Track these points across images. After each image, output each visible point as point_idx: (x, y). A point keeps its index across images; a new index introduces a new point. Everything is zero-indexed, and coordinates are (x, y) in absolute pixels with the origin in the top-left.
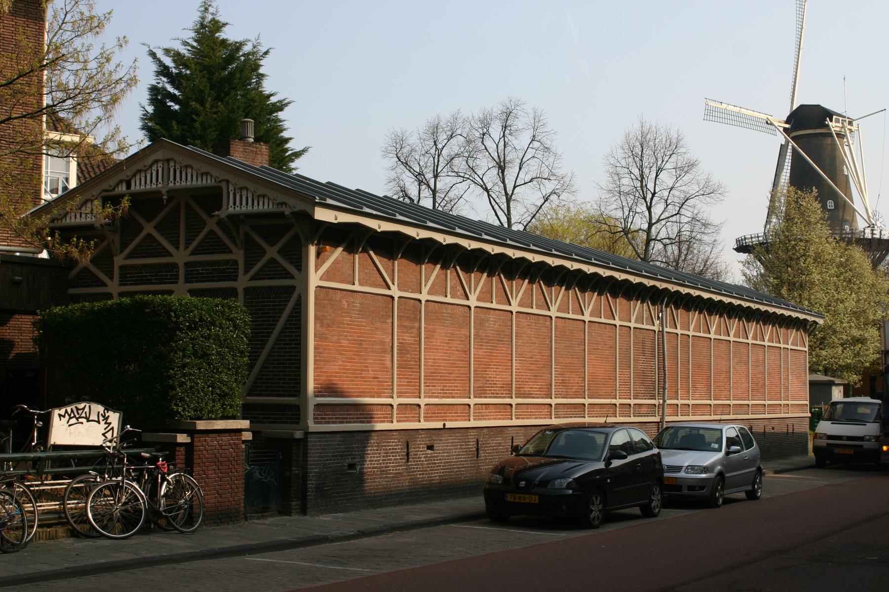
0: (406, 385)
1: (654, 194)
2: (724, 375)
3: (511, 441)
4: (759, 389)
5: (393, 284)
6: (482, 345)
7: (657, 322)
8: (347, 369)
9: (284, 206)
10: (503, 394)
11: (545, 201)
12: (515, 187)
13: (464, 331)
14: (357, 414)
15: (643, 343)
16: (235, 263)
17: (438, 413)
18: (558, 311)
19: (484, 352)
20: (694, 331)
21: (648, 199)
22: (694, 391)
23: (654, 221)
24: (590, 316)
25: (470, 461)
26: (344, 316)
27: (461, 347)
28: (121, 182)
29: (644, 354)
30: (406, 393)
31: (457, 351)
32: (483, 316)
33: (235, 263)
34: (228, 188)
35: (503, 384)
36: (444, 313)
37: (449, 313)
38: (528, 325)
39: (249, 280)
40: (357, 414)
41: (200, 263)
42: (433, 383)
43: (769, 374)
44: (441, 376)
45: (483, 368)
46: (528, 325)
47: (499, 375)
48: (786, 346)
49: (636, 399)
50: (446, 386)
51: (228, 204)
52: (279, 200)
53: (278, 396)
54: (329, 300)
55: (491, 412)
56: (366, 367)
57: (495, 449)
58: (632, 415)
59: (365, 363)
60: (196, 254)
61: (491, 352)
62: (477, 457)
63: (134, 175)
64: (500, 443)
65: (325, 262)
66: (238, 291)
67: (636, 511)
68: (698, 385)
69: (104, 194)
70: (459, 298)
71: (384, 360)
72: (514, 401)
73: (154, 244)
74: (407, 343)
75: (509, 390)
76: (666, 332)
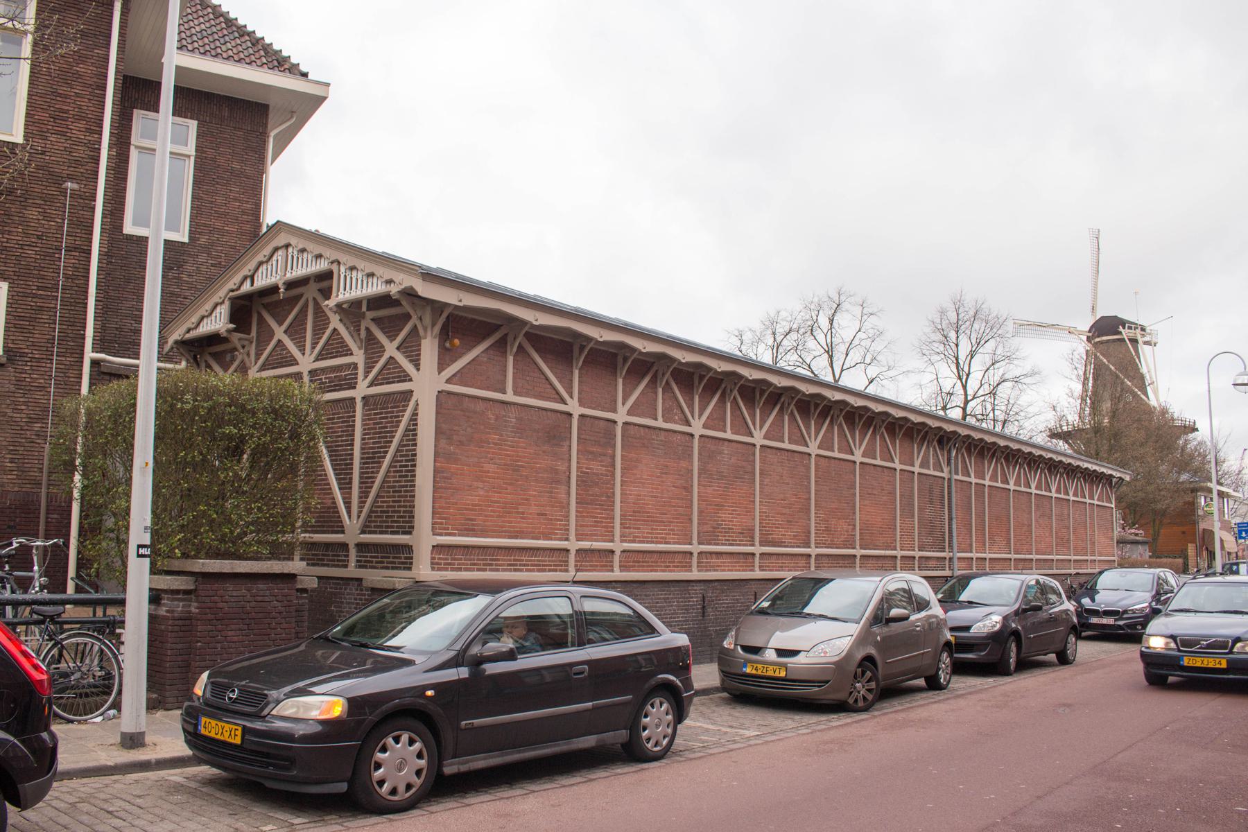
0: (591, 526)
1: (968, 375)
2: (1025, 528)
3: (753, 597)
4: (1063, 545)
5: (572, 397)
6: (711, 482)
7: (946, 469)
8: (492, 502)
9: (392, 285)
10: (742, 541)
11: (870, 383)
12: (842, 371)
13: (684, 464)
14: (510, 560)
15: (931, 491)
16: (355, 366)
17: (643, 562)
18: (819, 448)
19: (714, 490)
20: (990, 480)
21: (964, 381)
22: (991, 544)
23: (969, 398)
24: (862, 456)
25: (692, 621)
26: (489, 433)
27: (679, 483)
28: (245, 278)
29: (931, 502)
30: (592, 535)
31: (674, 486)
32: (713, 448)
33: (355, 366)
34: (339, 271)
35: (743, 529)
36: (653, 440)
37: (661, 441)
38: (778, 462)
39: (368, 387)
40: (510, 560)
41: (323, 370)
42: (635, 524)
43: (1075, 529)
44: (648, 517)
45: (714, 509)
46: (778, 462)
47: (736, 518)
48: (1091, 502)
49: (922, 551)
50: (655, 529)
51: (338, 290)
52: (387, 277)
53: (393, 533)
54: (462, 410)
55: (725, 562)
56: (527, 500)
57: (731, 607)
58: (917, 569)
59: (525, 495)
60: (322, 359)
61: (724, 491)
62: (703, 616)
63: (257, 269)
64: (737, 600)
65: (456, 360)
66: (357, 401)
67: (921, 682)
68: (996, 538)
69: (231, 294)
70: (675, 422)
71: (557, 493)
72: (758, 549)
73: (284, 352)
74: (594, 474)
75: (750, 537)
76: (956, 480)
